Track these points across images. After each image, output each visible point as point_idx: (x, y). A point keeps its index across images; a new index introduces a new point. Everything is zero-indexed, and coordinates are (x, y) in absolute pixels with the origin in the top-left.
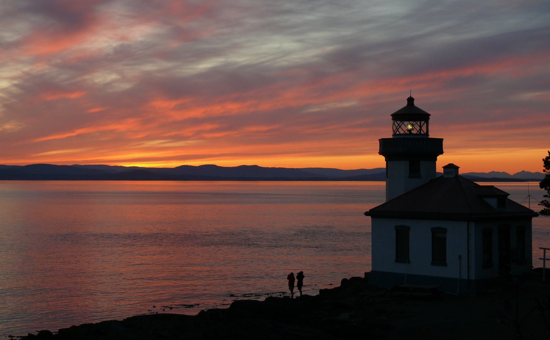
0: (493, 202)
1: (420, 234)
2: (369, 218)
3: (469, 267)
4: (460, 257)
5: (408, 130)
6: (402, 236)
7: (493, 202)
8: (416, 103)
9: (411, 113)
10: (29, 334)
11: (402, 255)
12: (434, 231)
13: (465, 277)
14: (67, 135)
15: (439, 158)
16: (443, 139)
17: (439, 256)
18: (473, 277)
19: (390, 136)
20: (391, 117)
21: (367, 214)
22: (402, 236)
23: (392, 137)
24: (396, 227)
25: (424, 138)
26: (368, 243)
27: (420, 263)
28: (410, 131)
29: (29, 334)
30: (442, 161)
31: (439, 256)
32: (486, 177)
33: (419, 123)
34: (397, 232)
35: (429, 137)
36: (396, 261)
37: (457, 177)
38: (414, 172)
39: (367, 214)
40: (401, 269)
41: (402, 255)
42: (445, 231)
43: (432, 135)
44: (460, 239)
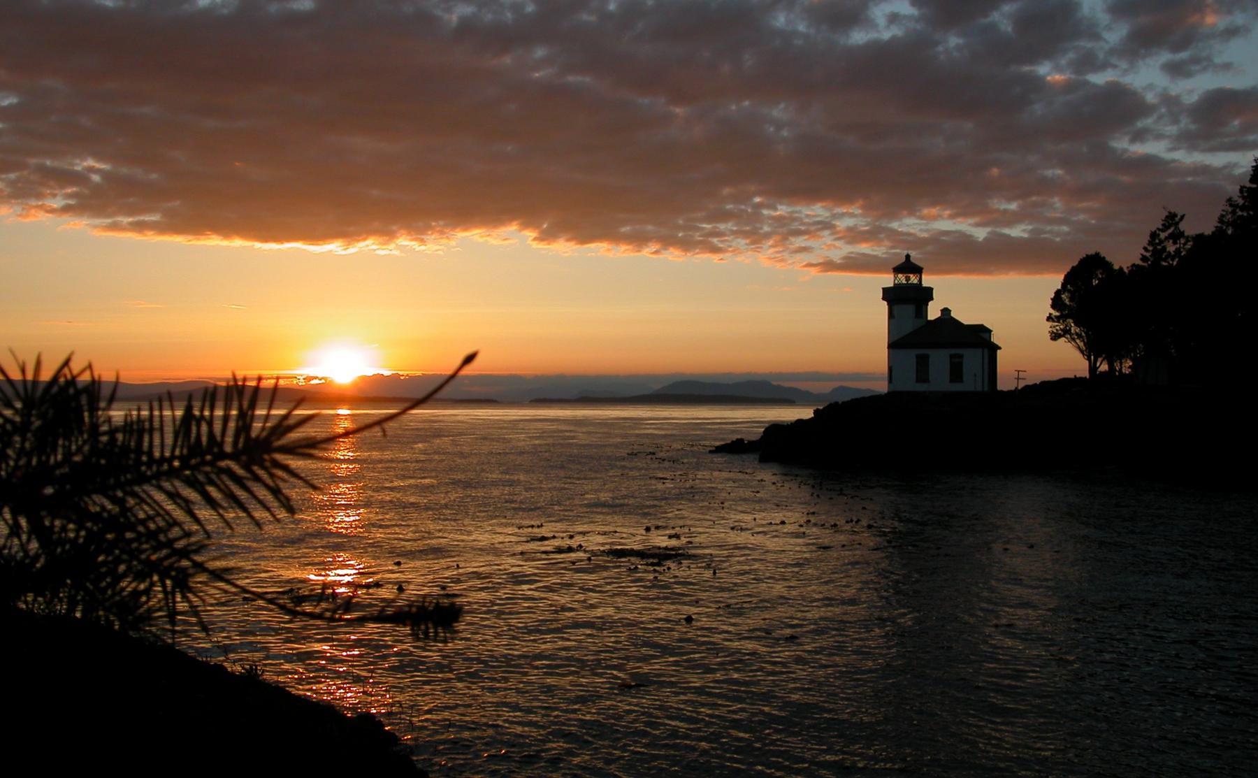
12: (952, 356)
17: (956, 373)
27: (940, 380)
31: (956, 373)
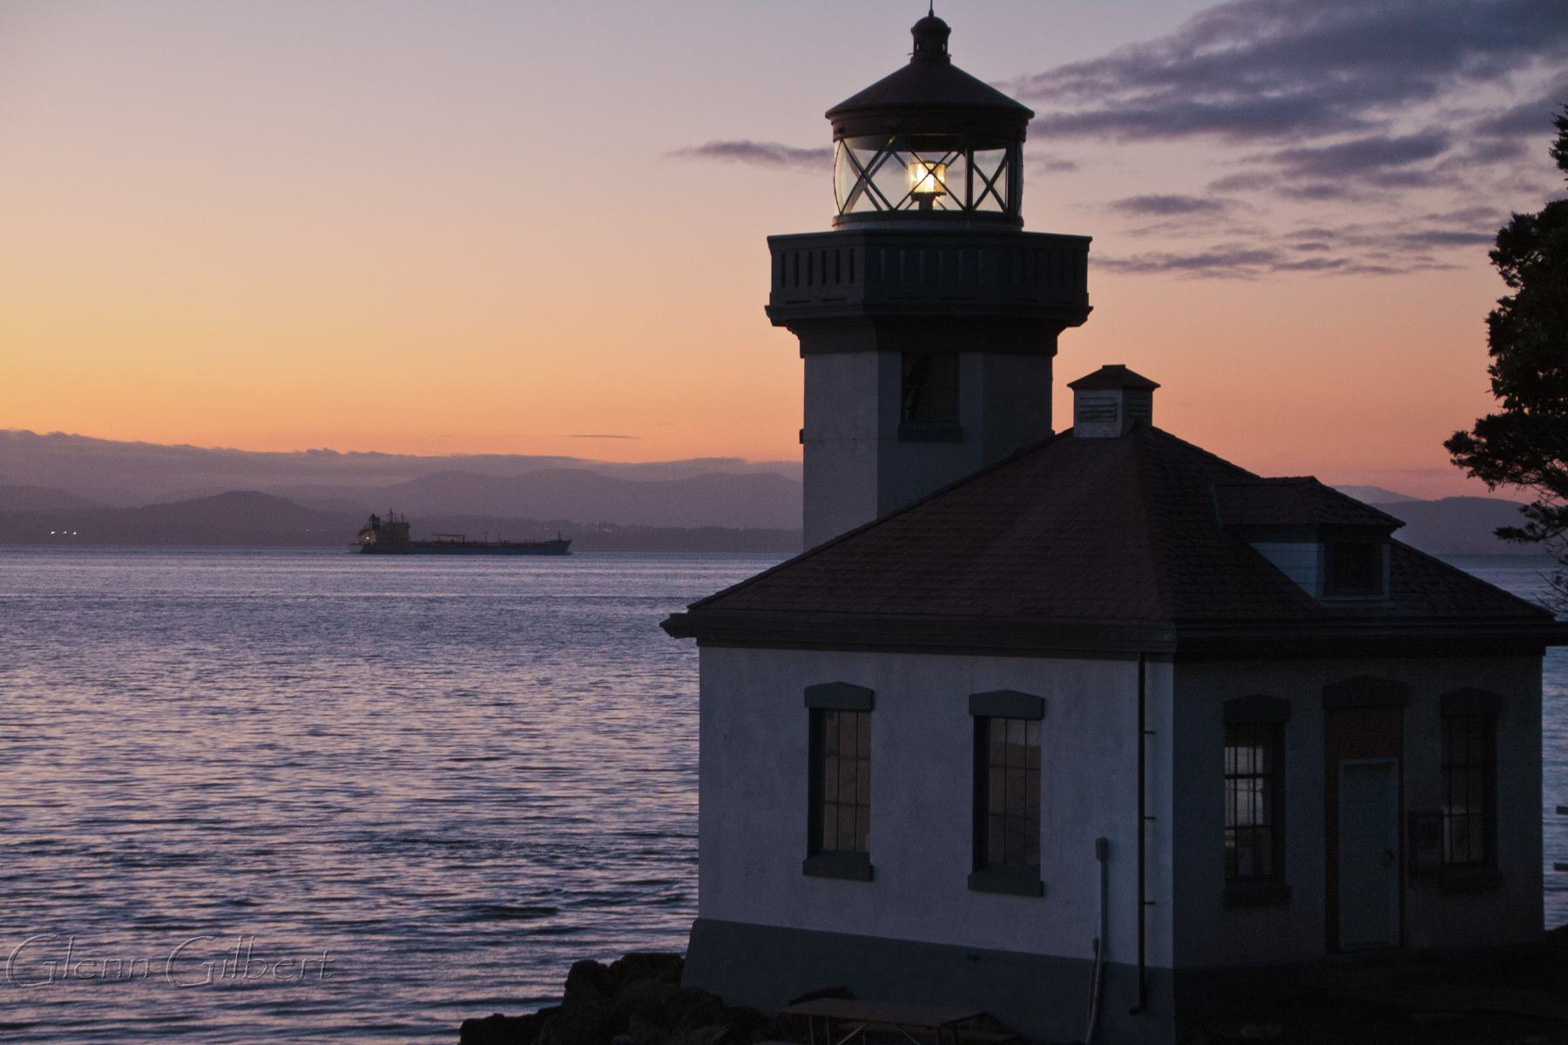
0: (1301, 562)
2: (690, 649)
4: (1104, 849)
5: (916, 196)
7: (1301, 562)
8: (963, 55)
9: (930, 103)
10: (1091, 308)
15: (1067, 339)
16: (1089, 239)
17: (1004, 852)
19: (819, 219)
21: (675, 627)
23: (833, 229)
28: (926, 199)
29: (1091, 308)
30: (1076, 354)
31: (1004, 852)
33: (961, 161)
35: (1024, 229)
38: (919, 409)
39: (675, 627)
40: (834, 910)
43: (1037, 218)
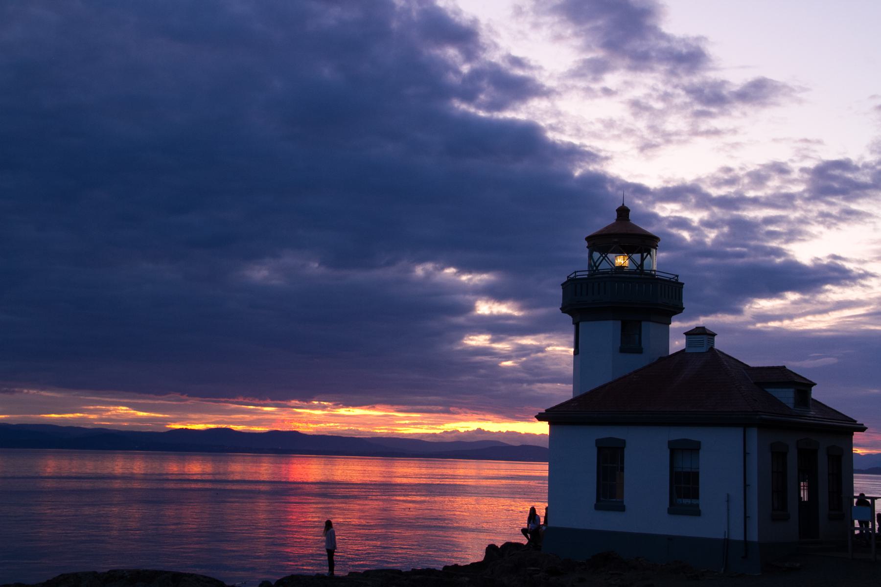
0: (786, 396)
1: (647, 454)
3: (746, 517)
6: (610, 459)
7: (786, 396)
11: (609, 490)
12: (676, 449)
13: (737, 535)
14: (156, 402)
17: (684, 488)
18: (754, 537)
20: (586, 244)
22: (610, 459)
24: (598, 441)
25: (640, 277)
26: (546, 485)
27: (646, 509)
31: (684, 488)
32: (777, 313)
34: (600, 450)
36: (597, 507)
37: (713, 353)
38: (630, 343)
41: (609, 490)
42: (694, 448)
44: (726, 461)
